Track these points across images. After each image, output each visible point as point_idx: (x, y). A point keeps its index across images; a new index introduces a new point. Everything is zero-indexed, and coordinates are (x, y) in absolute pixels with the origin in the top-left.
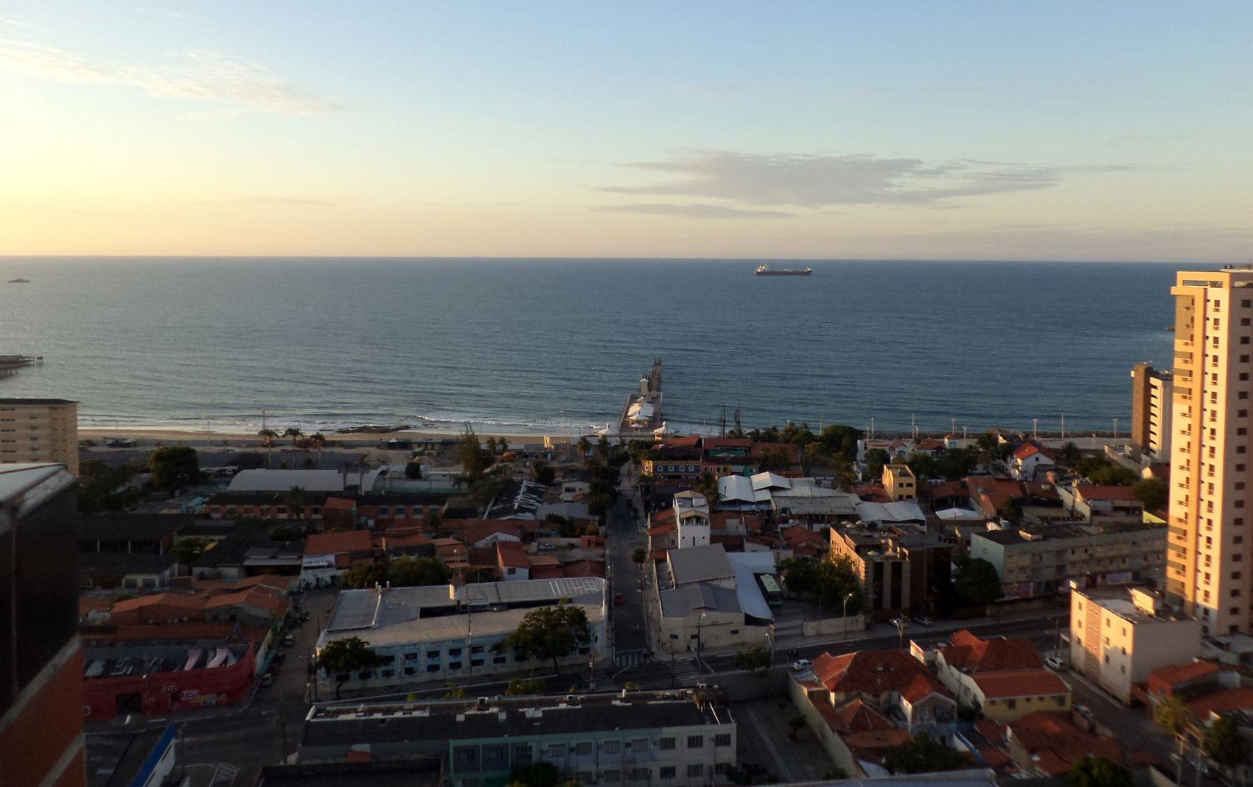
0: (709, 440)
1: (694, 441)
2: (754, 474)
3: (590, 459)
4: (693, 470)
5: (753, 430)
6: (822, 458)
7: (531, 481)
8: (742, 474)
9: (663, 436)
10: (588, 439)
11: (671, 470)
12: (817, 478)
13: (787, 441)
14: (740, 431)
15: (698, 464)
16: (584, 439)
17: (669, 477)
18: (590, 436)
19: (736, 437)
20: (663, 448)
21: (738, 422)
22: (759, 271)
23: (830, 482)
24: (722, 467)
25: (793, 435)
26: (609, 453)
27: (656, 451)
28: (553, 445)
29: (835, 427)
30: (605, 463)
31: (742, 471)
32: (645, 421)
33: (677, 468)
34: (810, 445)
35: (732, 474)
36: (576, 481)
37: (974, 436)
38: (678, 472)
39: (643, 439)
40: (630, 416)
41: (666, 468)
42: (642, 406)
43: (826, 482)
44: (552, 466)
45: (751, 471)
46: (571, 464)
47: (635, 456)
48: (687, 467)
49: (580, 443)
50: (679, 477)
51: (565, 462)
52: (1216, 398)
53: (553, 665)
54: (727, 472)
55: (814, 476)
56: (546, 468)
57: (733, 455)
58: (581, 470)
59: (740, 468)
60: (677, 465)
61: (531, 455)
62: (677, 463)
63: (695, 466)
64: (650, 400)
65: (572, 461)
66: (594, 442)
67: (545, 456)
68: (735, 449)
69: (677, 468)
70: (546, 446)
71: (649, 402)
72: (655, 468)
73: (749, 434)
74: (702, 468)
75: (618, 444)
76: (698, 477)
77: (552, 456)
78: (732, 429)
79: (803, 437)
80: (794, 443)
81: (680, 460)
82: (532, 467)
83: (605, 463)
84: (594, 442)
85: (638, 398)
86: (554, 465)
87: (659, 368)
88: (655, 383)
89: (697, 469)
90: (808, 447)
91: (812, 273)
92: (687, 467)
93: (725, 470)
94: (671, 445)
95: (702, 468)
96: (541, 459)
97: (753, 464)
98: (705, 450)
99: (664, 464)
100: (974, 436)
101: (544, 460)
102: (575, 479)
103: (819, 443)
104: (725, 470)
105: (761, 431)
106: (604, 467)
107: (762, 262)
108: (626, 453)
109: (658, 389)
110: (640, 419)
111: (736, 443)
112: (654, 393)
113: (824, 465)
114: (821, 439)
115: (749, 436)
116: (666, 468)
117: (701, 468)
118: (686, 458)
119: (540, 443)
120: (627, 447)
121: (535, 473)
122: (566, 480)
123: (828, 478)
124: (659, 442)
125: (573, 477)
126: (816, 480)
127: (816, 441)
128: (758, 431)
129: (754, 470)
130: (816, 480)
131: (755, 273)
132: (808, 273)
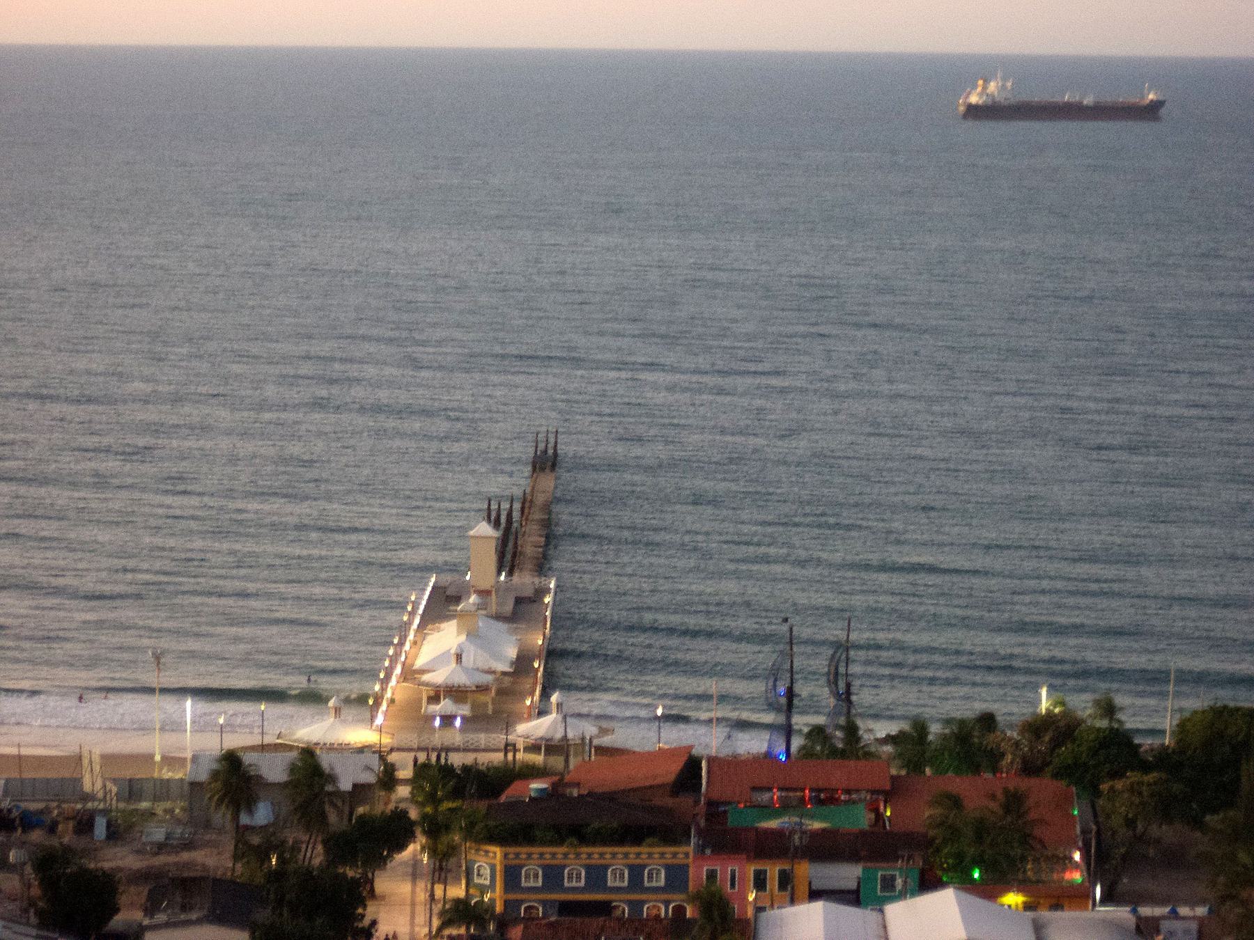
0: (727, 766)
1: (670, 771)
2: (902, 896)
3: (256, 840)
4: (662, 883)
5: (905, 726)
6: (1167, 833)
7: (28, 924)
8: (852, 897)
9: (552, 747)
10: (248, 759)
11: (575, 881)
12: (1146, 911)
13: (1030, 768)
14: (851, 731)
15: (680, 859)
16: (231, 760)
17: (567, 908)
18: (263, 748)
19: (835, 753)
20: (544, 796)
21: (845, 697)
22: (974, 99)
23: (1194, 926)
24: (773, 871)
25: (1056, 743)
26: (333, 817)
27: (514, 805)
28: (115, 781)
29: (1220, 713)
30: (315, 856)
31: (852, 885)
32: (483, 689)
33: (596, 876)
34: (1119, 785)
35: (815, 895)
36: (199, 922)
37: (904, 718)
38: (603, 887)
39: (468, 759)
40: (423, 671)
41: (553, 876)
42: (472, 635)
43: (1177, 925)
44: (107, 865)
45: (888, 884)
46: (186, 856)
47: (435, 829)
48: (636, 872)
49: (215, 775)
50: (604, 908)
51: (161, 848)
52: (1168, 673)
53: (409, 896)
54: (790, 890)
55: (1134, 900)
56: (84, 872)
57: (817, 825)
58: (217, 882)
59: (847, 874)
60: (596, 860)
61: (28, 821)
62: (598, 854)
63: (668, 868)
64: (509, 607)
65: (189, 845)
66: (275, 770)
67: (84, 824)
68: (826, 799)
69: (596, 876)
70: (87, 787)
71: (498, 617)
72: (512, 876)
73: (889, 739)
74: (698, 873)
75: (369, 778)
76: (680, 910)
77: (109, 825)
78: (820, 720)
79: (1094, 753)
80: (1056, 776)
81: (604, 843)
82: (28, 869)
83: (315, 856)
84: (275, 770)
85: (457, 599)
86: (120, 859)
87: (547, 482)
88: (531, 542)
89: (677, 876)
90: (1112, 788)
91: (1163, 111)
92: (636, 872)
93: (786, 880)
94: (578, 785)
95: (698, 873)
96: (67, 835)
97: (896, 859)
98: (711, 804)
99: (548, 860)
100: (904, 718)
101: (80, 843)
102: (194, 916)
103: (1151, 777)
104: (786, 880)
105: (935, 729)
106: (309, 871)
107: (981, 68)
108: (401, 815)
109: (541, 567)
110: (462, 679)
111: (837, 775)
112: (525, 580)
113: (1173, 860)
114: (1163, 759)
115: (888, 749)
116: (553, 876)
117: (691, 871)
118: (632, 835)
119: (66, 774)
120: (403, 791)
121: (36, 891)
122: (161, 917)
123: (1184, 911)
124: (531, 772)
125: (184, 908)
126: (1139, 918)
127: (1145, 767)
128: (920, 727)
129: (899, 882)
130: (1139, 918)
131: (962, 109)
132: (1151, 111)
